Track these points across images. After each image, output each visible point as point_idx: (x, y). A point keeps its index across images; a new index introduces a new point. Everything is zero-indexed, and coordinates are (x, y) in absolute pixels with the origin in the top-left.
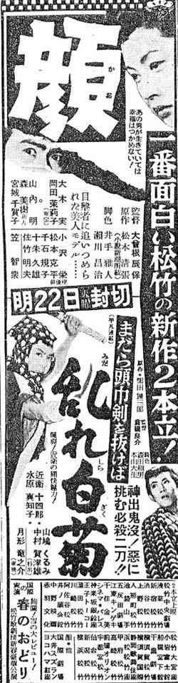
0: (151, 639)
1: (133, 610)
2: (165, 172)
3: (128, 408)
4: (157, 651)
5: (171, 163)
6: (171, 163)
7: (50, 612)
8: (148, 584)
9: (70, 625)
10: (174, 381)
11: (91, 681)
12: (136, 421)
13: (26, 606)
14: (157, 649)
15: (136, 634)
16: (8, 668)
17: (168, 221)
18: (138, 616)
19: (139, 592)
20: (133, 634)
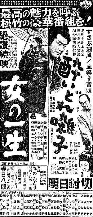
0: (45, 196)
1: (76, 207)
2: (60, 25)
3: (21, 156)
4: (48, 202)
5: (62, 20)
6: (62, 20)
7: (53, 208)
8: (83, 195)
9: (27, 214)
10: (69, 120)
11: (33, 215)
12: (80, 73)
13: (5, 169)
14: (48, 201)
15: (42, 194)
16: (47, 180)
17: (32, 122)
18: (78, 210)
19: (79, 199)
20: (40, 194)
